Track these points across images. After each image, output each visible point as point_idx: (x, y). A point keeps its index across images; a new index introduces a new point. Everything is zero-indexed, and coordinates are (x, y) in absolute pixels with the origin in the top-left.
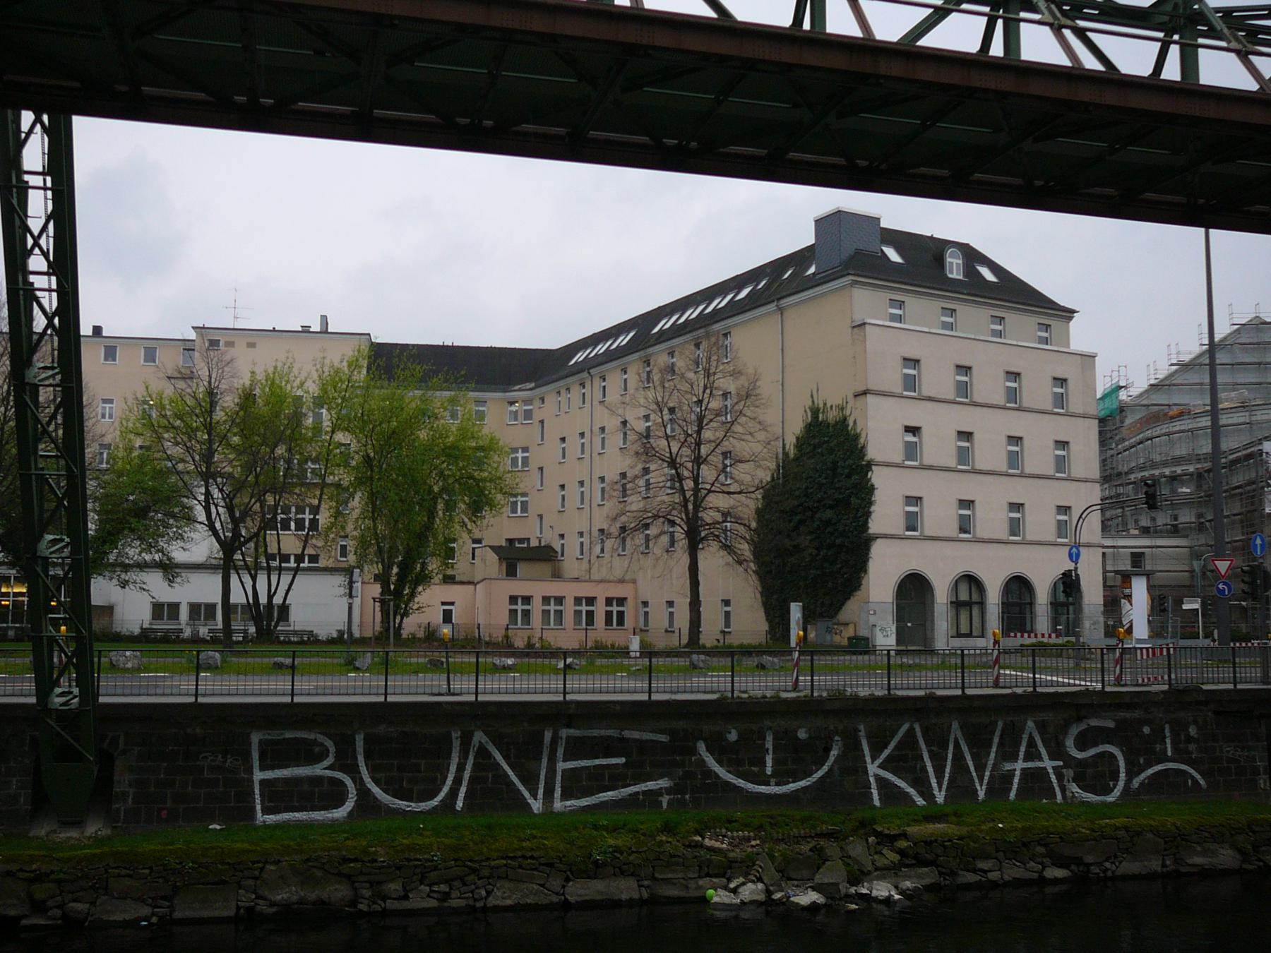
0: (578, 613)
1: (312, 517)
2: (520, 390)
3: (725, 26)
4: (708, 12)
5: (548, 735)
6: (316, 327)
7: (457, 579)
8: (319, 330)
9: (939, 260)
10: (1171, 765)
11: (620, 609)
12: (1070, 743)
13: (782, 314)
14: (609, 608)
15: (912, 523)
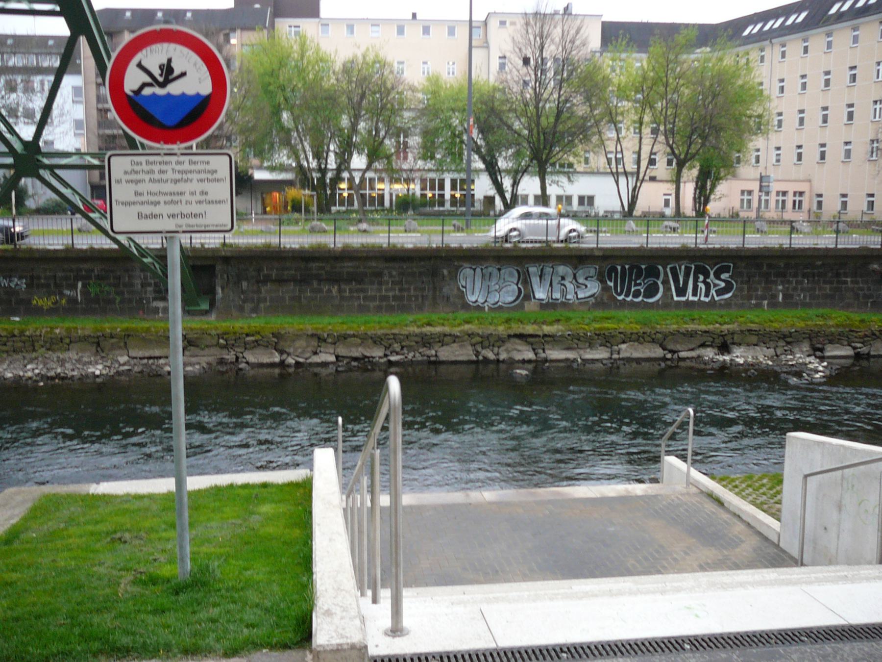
0: (777, 201)
7: (658, 178)
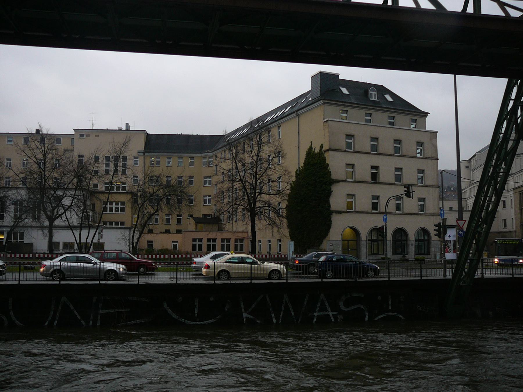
1: (107, 206)
2: (208, 152)
3: (396, 9)
4: (413, 5)
5: (94, 300)
6: (124, 128)
8: (125, 129)
9: (366, 93)
10: (390, 314)
11: (242, 243)
12: (341, 304)
13: (298, 118)
14: (236, 243)
15: (350, 205)
